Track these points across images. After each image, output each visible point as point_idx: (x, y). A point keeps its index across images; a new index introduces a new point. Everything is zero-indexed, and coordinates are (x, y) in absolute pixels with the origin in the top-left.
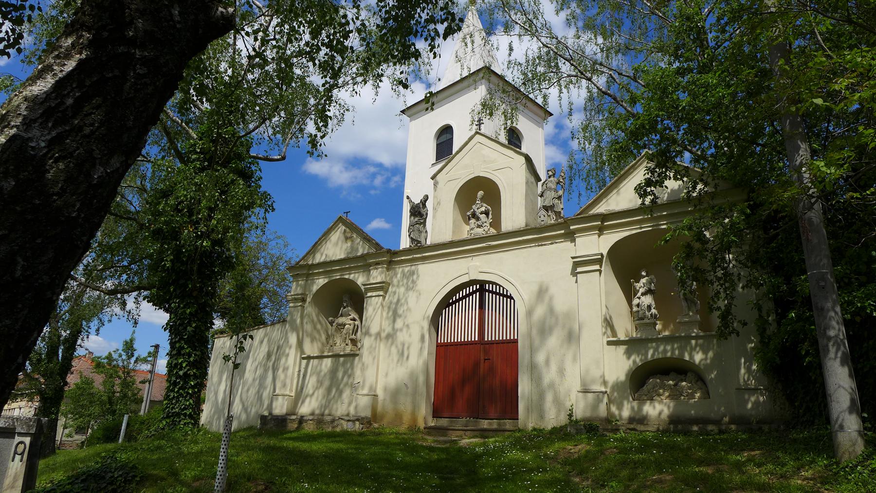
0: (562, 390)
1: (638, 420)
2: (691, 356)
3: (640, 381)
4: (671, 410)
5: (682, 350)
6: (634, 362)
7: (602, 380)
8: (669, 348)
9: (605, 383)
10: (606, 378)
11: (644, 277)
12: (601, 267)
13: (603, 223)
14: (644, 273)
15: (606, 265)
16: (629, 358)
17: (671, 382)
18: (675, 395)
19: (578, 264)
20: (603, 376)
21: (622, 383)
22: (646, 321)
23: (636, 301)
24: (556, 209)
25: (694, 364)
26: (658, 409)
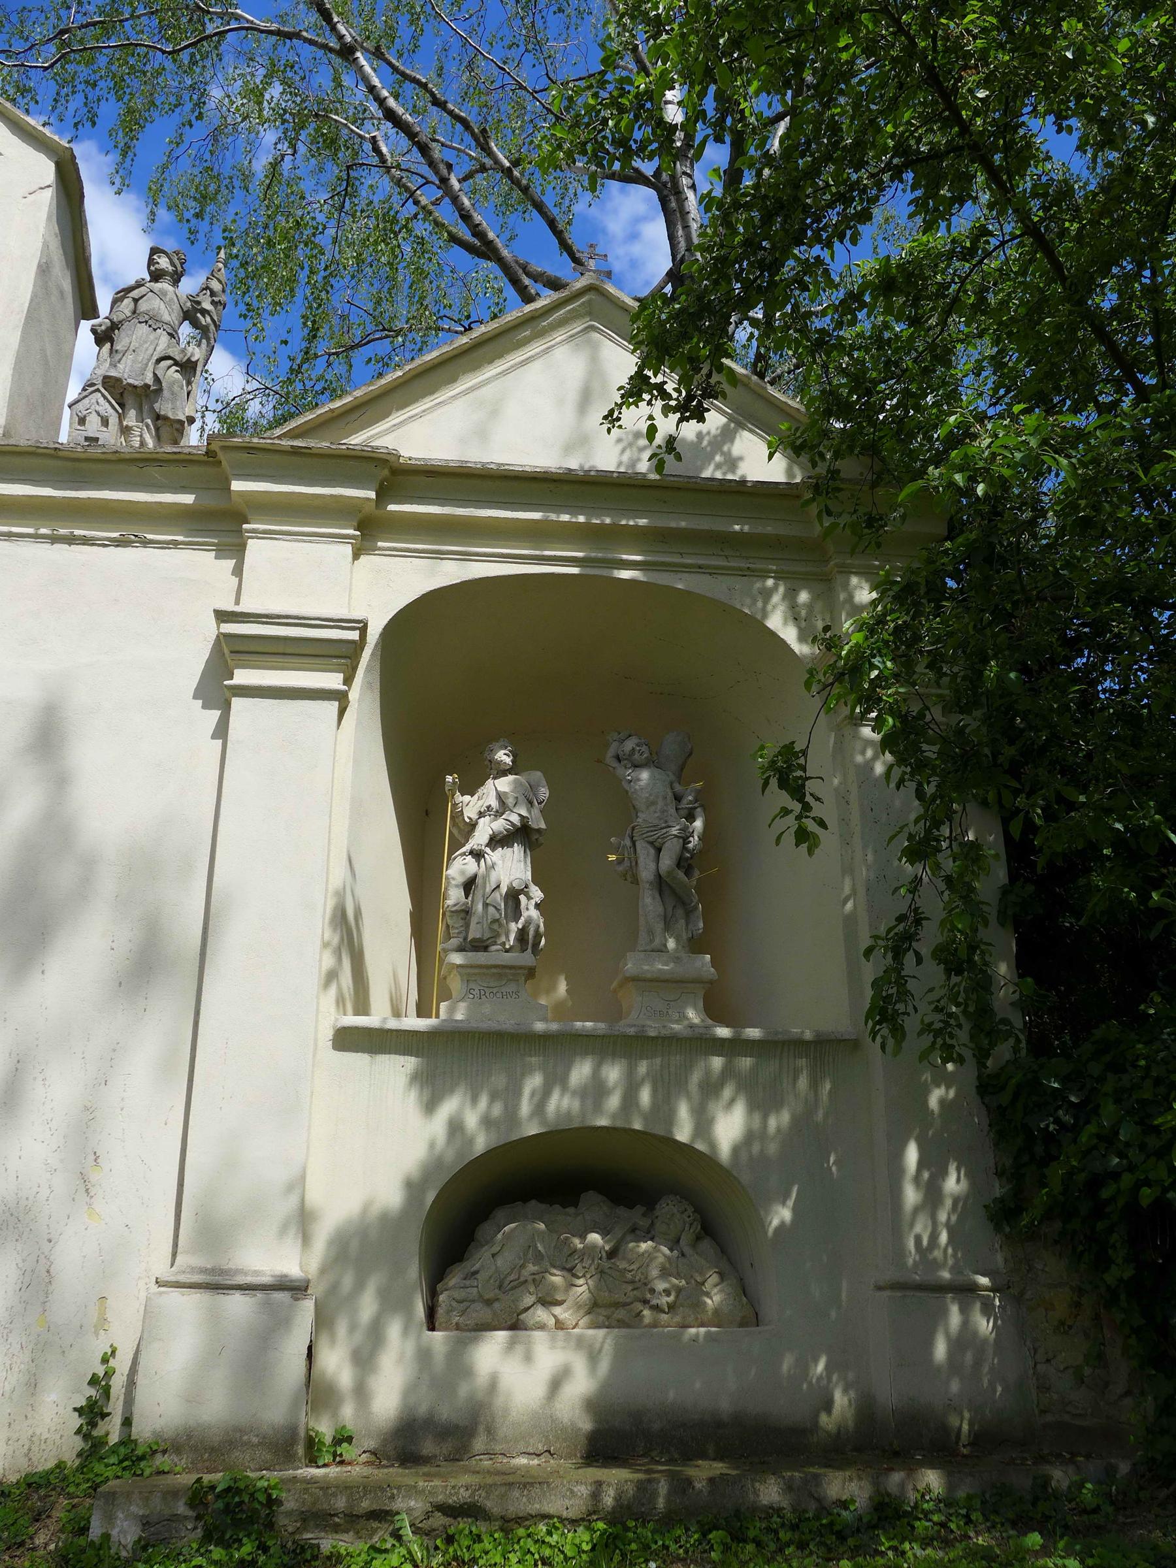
0: (74, 1251)
1: (432, 1437)
2: (703, 1125)
3: (467, 1231)
4: (604, 1366)
5: (668, 1089)
6: (455, 1127)
7: (293, 1201)
8: (613, 1073)
9: (303, 1220)
10: (315, 1195)
11: (504, 773)
12: (348, 681)
13: (390, 500)
14: (503, 756)
15: (368, 685)
16: (430, 1107)
17: (595, 1238)
18: (615, 1307)
19: (241, 653)
20: (298, 1183)
21: (385, 1218)
22: (495, 956)
23: (459, 868)
24: (164, 407)
25: (708, 1161)
26: (540, 1372)
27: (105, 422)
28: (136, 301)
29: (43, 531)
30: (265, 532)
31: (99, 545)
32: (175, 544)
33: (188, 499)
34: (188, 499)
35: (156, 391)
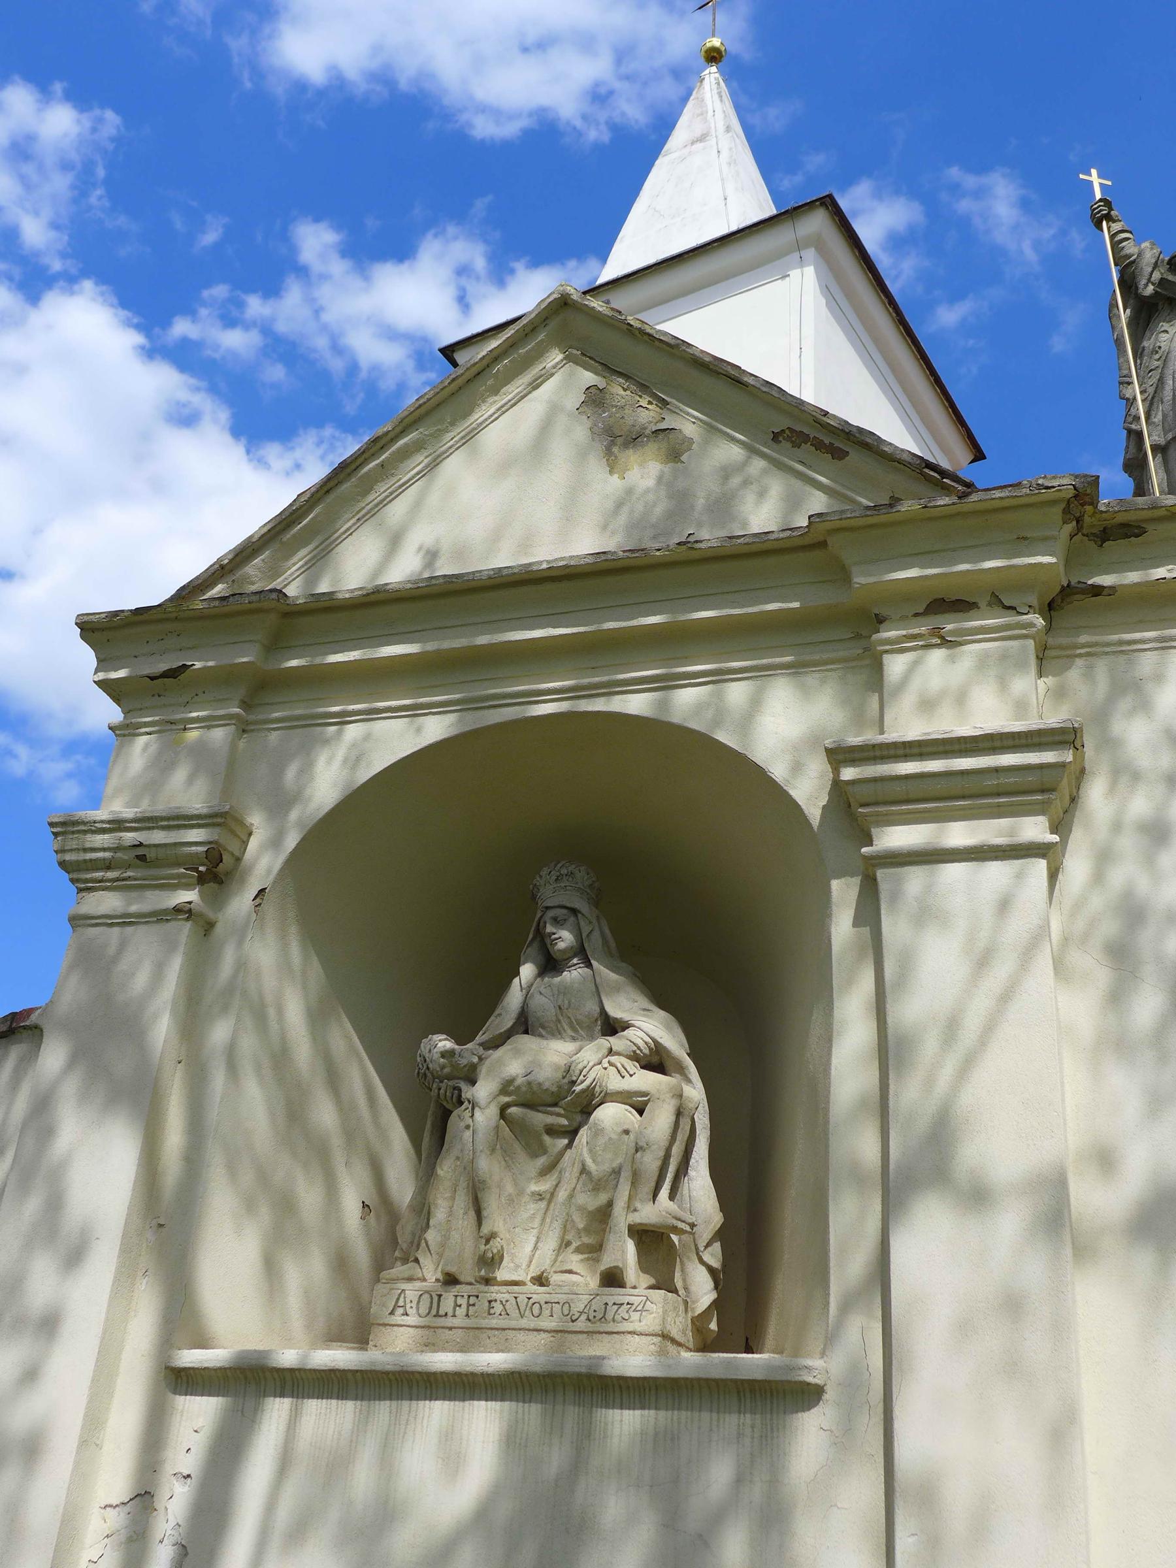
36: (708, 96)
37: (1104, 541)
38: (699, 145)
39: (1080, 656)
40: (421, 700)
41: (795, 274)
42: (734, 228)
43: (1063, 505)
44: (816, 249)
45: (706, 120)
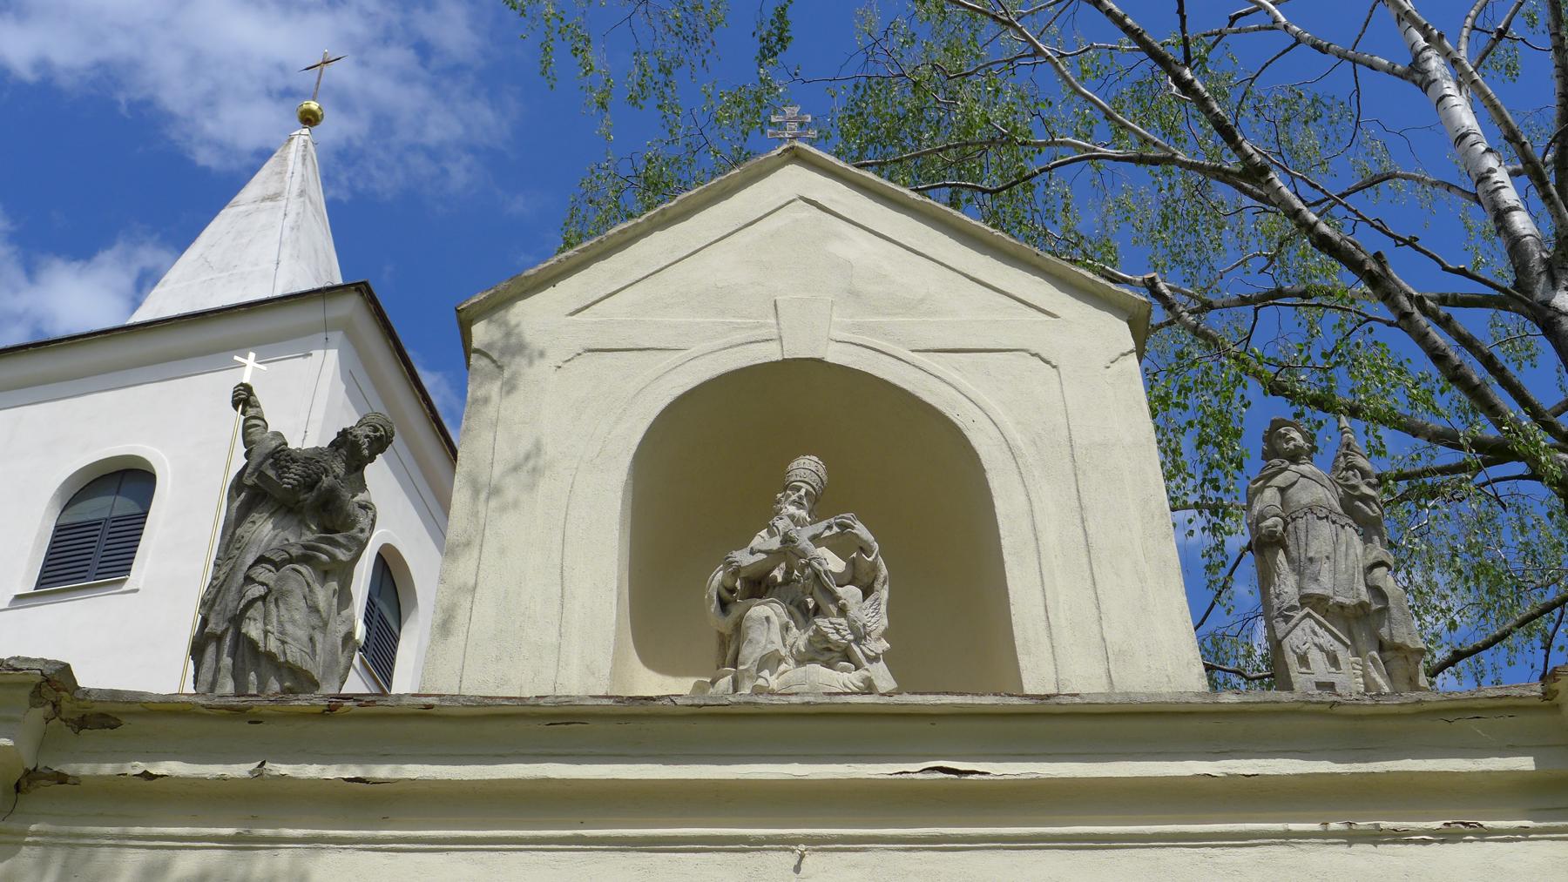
27: (1334, 660)
28: (1282, 491)
29: (1334, 826)
30: (770, 840)
31: (1417, 842)
32: (1525, 833)
33: (1526, 763)
34: (1526, 763)
35: (1380, 611)
36: (292, 156)
37: (81, 728)
38: (269, 204)
39: (28, 844)
40: (382, 771)
41: (318, 354)
42: (279, 293)
43: (31, 689)
44: (346, 333)
45: (282, 180)
